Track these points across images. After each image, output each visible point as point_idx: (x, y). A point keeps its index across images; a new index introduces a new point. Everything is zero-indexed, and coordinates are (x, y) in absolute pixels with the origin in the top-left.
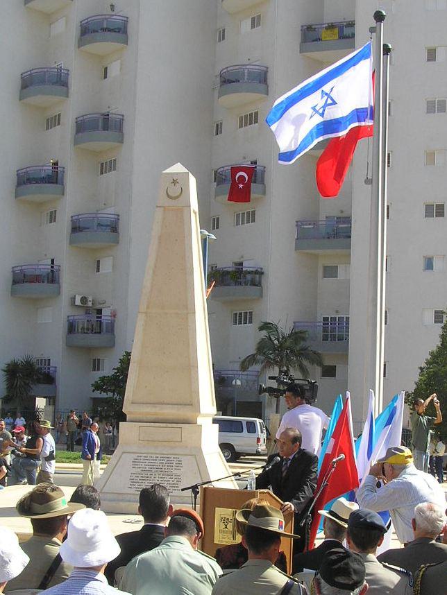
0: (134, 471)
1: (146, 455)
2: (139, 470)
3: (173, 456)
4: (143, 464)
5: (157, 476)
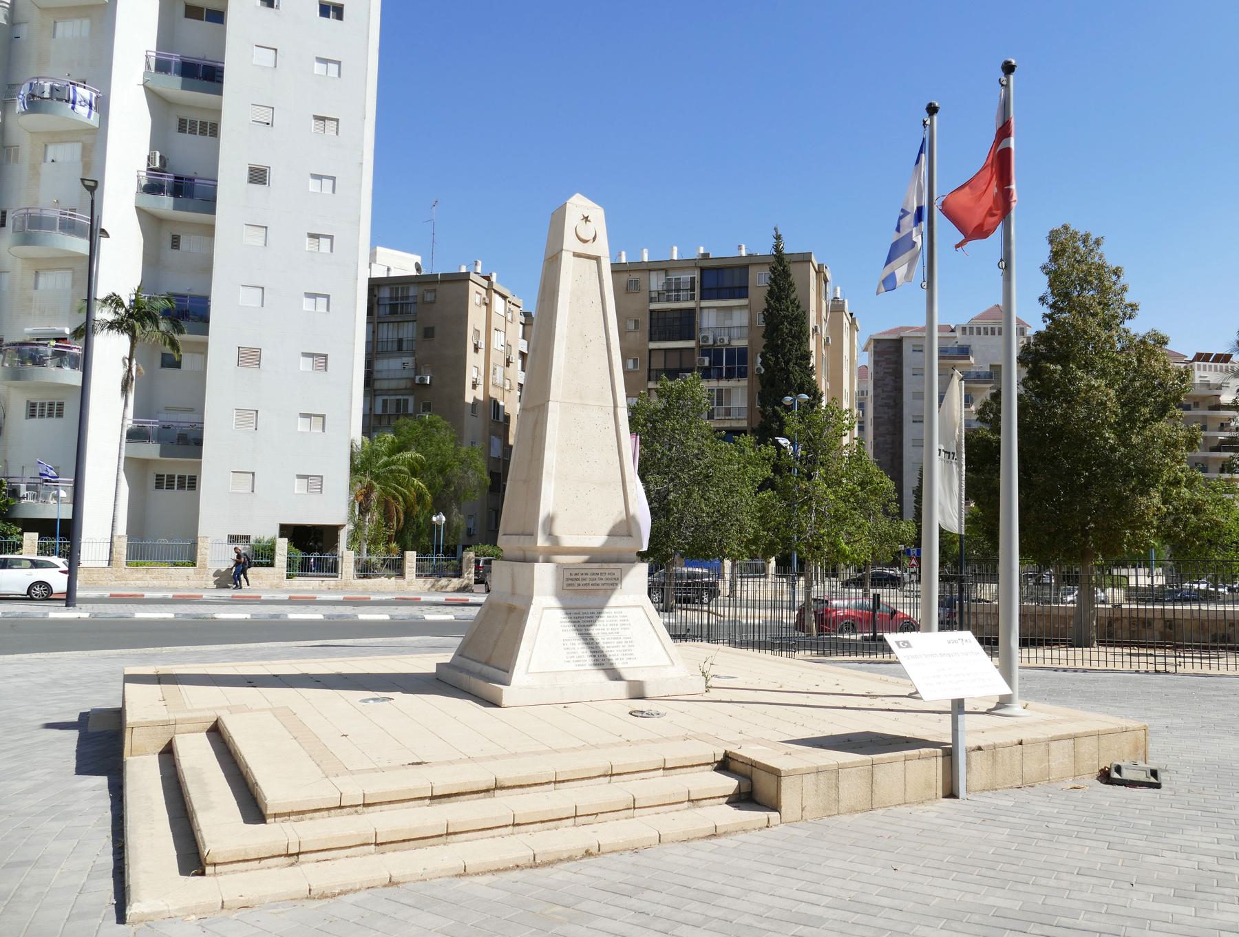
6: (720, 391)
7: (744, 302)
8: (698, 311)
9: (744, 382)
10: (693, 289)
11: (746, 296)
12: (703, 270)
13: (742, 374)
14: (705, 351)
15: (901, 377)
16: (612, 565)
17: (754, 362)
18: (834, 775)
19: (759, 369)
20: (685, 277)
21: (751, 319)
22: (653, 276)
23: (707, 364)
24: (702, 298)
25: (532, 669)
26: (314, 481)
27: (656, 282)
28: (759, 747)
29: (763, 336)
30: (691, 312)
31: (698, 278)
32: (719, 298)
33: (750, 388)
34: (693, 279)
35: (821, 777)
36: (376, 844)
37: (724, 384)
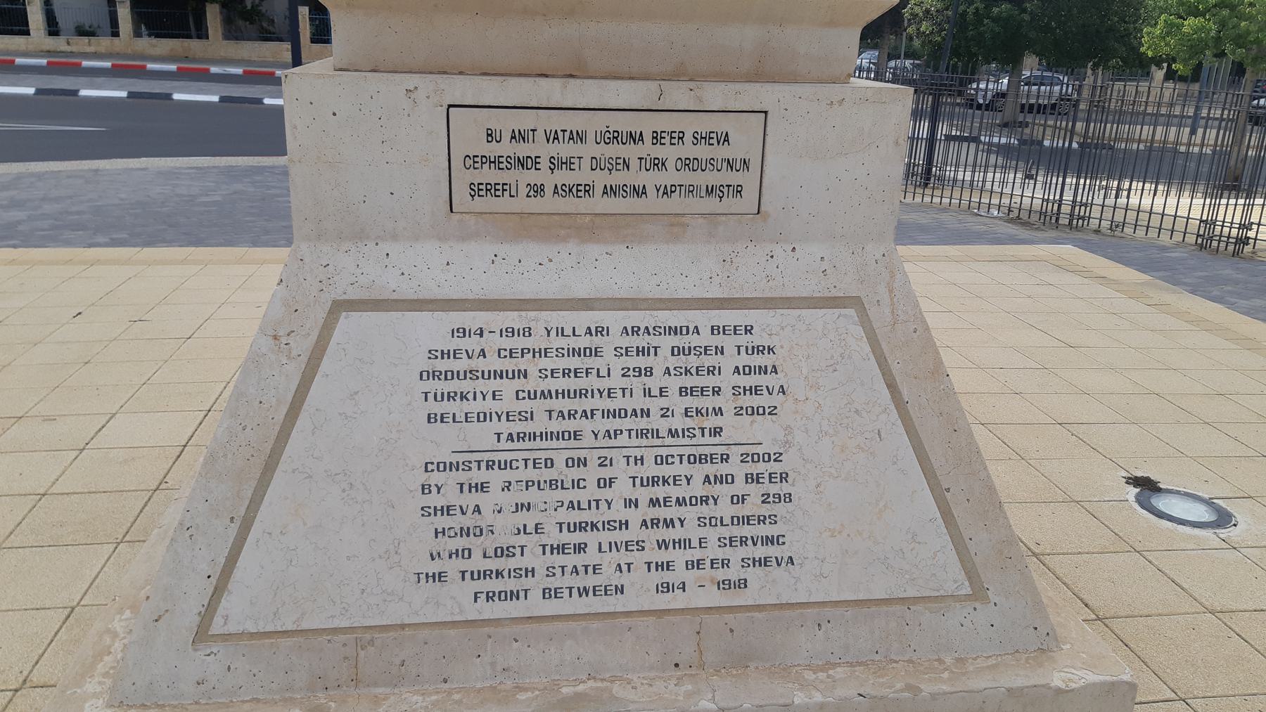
1: (513, 319)
3: (705, 319)
4: (508, 387)
5: (621, 470)
16: (715, 95)
25: (236, 612)
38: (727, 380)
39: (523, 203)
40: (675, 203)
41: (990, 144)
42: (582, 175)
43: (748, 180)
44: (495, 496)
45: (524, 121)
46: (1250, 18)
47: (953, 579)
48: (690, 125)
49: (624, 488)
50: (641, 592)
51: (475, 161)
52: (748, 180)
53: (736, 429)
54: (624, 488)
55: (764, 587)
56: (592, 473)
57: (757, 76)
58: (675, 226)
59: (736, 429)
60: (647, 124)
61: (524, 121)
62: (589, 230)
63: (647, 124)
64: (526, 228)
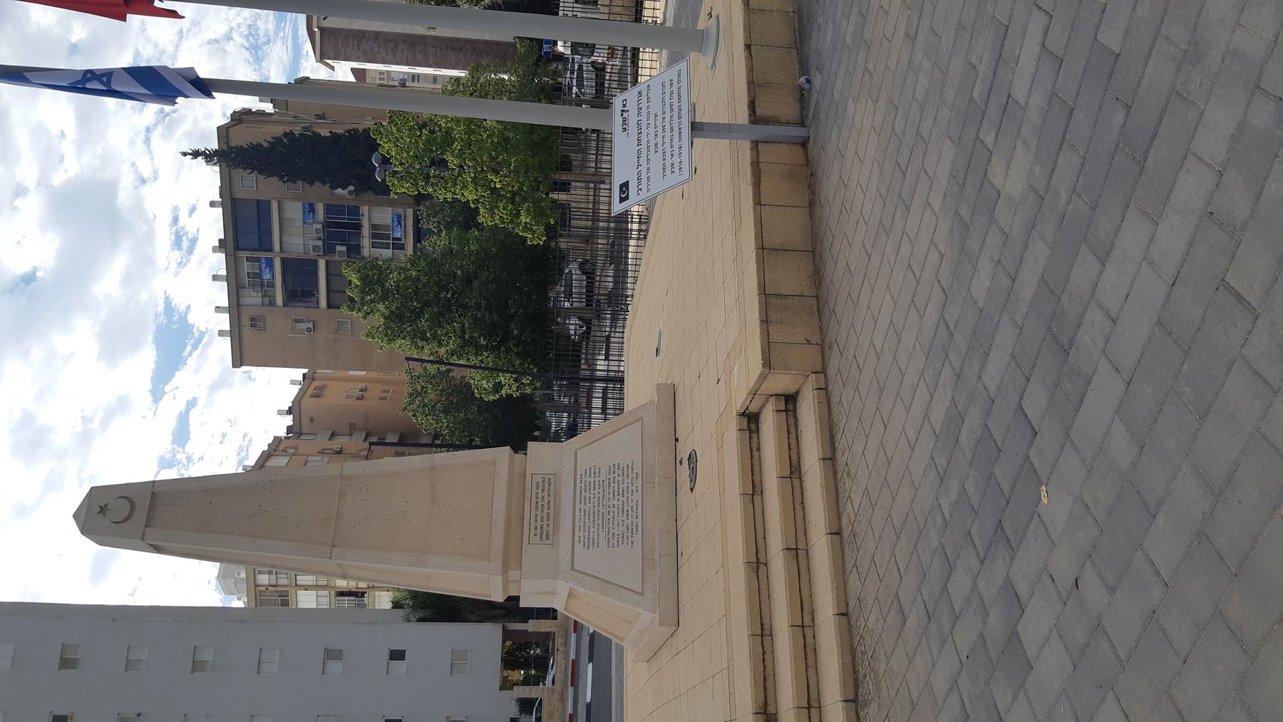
0: (603, 543)
2: (602, 535)
6: (374, 236)
7: (274, 205)
8: (284, 255)
9: (365, 209)
10: (258, 260)
11: (268, 203)
12: (237, 248)
13: (355, 211)
14: (329, 250)
15: (364, 32)
16: (528, 485)
17: (342, 196)
18: (773, 301)
19: (350, 193)
20: (246, 267)
21: (293, 199)
22: (245, 301)
23: (344, 248)
24: (271, 250)
25: (638, 587)
26: (458, 660)
27: (252, 298)
28: (735, 371)
29: (311, 184)
30: (284, 261)
31: (248, 254)
32: (270, 232)
33: (371, 204)
34: (248, 259)
35: (772, 317)
36: (809, 709)
37: (366, 231)
38: (592, 480)
39: (551, 528)
40: (552, 493)
41: (611, 326)
42: (545, 515)
43: (547, 477)
44: (615, 531)
45: (533, 528)
46: (522, 185)
47: (638, 425)
48: (534, 490)
49: (615, 502)
50: (638, 497)
51: (541, 538)
52: (547, 477)
53: (603, 477)
54: (615, 502)
55: (638, 469)
56: (612, 510)
57: (525, 476)
58: (557, 493)
59: (603, 477)
60: (534, 500)
61: (533, 528)
62: (557, 513)
63: (534, 500)
64: (556, 528)
